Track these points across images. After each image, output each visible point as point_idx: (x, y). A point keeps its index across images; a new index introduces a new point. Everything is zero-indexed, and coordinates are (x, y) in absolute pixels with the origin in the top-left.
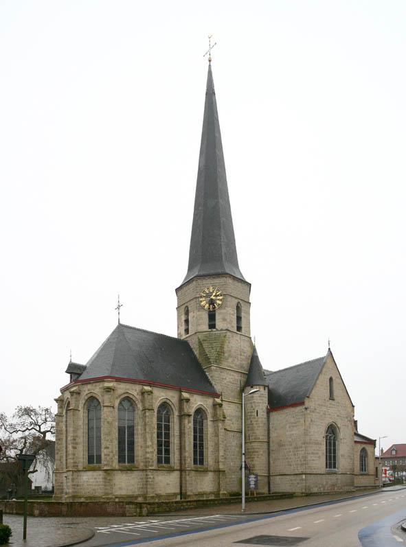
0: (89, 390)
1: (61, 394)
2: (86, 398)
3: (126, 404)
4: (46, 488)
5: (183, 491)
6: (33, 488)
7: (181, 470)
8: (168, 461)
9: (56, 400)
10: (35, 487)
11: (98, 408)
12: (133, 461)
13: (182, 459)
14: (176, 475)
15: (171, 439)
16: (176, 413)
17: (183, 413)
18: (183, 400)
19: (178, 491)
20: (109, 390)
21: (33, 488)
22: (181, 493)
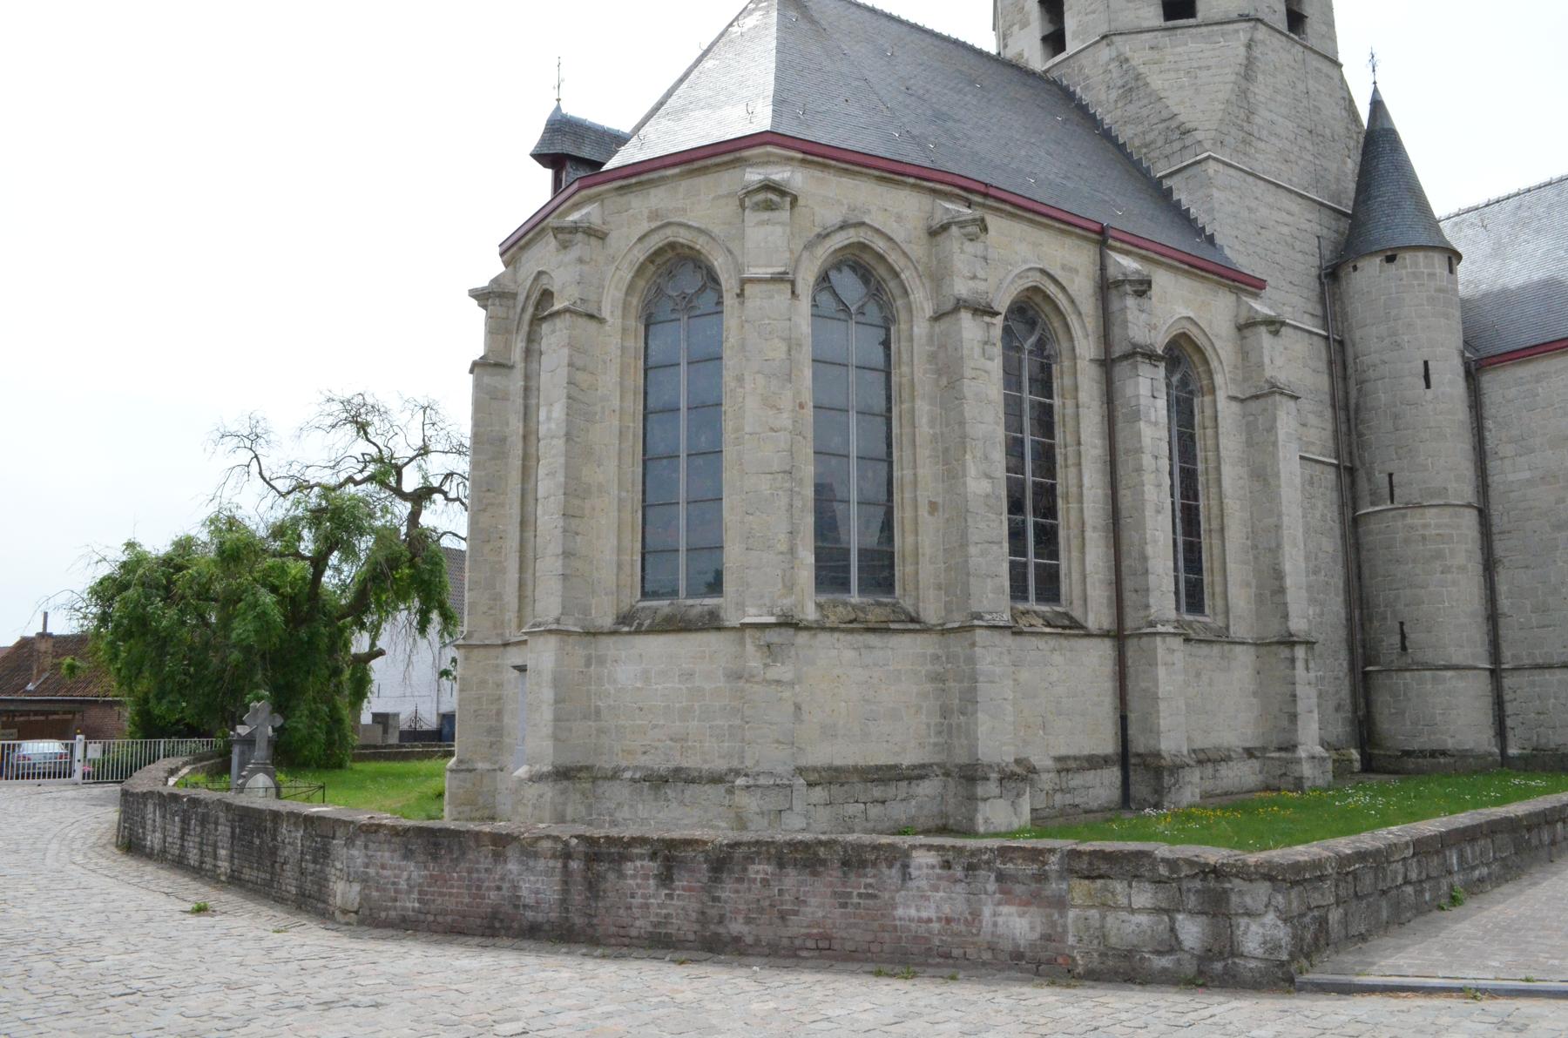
0: (654, 215)
1: (500, 268)
2: (640, 255)
3: (849, 286)
4: (416, 718)
5: (1139, 744)
6: (366, 718)
7: (1119, 636)
8: (1049, 586)
9: (482, 296)
10: (375, 716)
11: (706, 302)
12: (887, 585)
13: (1272, 587)
14: (1096, 657)
15: (1064, 479)
16: (1086, 347)
17: (1117, 352)
18: (1118, 284)
19: (1107, 745)
20: (774, 195)
21: (366, 718)
22: (1125, 757)
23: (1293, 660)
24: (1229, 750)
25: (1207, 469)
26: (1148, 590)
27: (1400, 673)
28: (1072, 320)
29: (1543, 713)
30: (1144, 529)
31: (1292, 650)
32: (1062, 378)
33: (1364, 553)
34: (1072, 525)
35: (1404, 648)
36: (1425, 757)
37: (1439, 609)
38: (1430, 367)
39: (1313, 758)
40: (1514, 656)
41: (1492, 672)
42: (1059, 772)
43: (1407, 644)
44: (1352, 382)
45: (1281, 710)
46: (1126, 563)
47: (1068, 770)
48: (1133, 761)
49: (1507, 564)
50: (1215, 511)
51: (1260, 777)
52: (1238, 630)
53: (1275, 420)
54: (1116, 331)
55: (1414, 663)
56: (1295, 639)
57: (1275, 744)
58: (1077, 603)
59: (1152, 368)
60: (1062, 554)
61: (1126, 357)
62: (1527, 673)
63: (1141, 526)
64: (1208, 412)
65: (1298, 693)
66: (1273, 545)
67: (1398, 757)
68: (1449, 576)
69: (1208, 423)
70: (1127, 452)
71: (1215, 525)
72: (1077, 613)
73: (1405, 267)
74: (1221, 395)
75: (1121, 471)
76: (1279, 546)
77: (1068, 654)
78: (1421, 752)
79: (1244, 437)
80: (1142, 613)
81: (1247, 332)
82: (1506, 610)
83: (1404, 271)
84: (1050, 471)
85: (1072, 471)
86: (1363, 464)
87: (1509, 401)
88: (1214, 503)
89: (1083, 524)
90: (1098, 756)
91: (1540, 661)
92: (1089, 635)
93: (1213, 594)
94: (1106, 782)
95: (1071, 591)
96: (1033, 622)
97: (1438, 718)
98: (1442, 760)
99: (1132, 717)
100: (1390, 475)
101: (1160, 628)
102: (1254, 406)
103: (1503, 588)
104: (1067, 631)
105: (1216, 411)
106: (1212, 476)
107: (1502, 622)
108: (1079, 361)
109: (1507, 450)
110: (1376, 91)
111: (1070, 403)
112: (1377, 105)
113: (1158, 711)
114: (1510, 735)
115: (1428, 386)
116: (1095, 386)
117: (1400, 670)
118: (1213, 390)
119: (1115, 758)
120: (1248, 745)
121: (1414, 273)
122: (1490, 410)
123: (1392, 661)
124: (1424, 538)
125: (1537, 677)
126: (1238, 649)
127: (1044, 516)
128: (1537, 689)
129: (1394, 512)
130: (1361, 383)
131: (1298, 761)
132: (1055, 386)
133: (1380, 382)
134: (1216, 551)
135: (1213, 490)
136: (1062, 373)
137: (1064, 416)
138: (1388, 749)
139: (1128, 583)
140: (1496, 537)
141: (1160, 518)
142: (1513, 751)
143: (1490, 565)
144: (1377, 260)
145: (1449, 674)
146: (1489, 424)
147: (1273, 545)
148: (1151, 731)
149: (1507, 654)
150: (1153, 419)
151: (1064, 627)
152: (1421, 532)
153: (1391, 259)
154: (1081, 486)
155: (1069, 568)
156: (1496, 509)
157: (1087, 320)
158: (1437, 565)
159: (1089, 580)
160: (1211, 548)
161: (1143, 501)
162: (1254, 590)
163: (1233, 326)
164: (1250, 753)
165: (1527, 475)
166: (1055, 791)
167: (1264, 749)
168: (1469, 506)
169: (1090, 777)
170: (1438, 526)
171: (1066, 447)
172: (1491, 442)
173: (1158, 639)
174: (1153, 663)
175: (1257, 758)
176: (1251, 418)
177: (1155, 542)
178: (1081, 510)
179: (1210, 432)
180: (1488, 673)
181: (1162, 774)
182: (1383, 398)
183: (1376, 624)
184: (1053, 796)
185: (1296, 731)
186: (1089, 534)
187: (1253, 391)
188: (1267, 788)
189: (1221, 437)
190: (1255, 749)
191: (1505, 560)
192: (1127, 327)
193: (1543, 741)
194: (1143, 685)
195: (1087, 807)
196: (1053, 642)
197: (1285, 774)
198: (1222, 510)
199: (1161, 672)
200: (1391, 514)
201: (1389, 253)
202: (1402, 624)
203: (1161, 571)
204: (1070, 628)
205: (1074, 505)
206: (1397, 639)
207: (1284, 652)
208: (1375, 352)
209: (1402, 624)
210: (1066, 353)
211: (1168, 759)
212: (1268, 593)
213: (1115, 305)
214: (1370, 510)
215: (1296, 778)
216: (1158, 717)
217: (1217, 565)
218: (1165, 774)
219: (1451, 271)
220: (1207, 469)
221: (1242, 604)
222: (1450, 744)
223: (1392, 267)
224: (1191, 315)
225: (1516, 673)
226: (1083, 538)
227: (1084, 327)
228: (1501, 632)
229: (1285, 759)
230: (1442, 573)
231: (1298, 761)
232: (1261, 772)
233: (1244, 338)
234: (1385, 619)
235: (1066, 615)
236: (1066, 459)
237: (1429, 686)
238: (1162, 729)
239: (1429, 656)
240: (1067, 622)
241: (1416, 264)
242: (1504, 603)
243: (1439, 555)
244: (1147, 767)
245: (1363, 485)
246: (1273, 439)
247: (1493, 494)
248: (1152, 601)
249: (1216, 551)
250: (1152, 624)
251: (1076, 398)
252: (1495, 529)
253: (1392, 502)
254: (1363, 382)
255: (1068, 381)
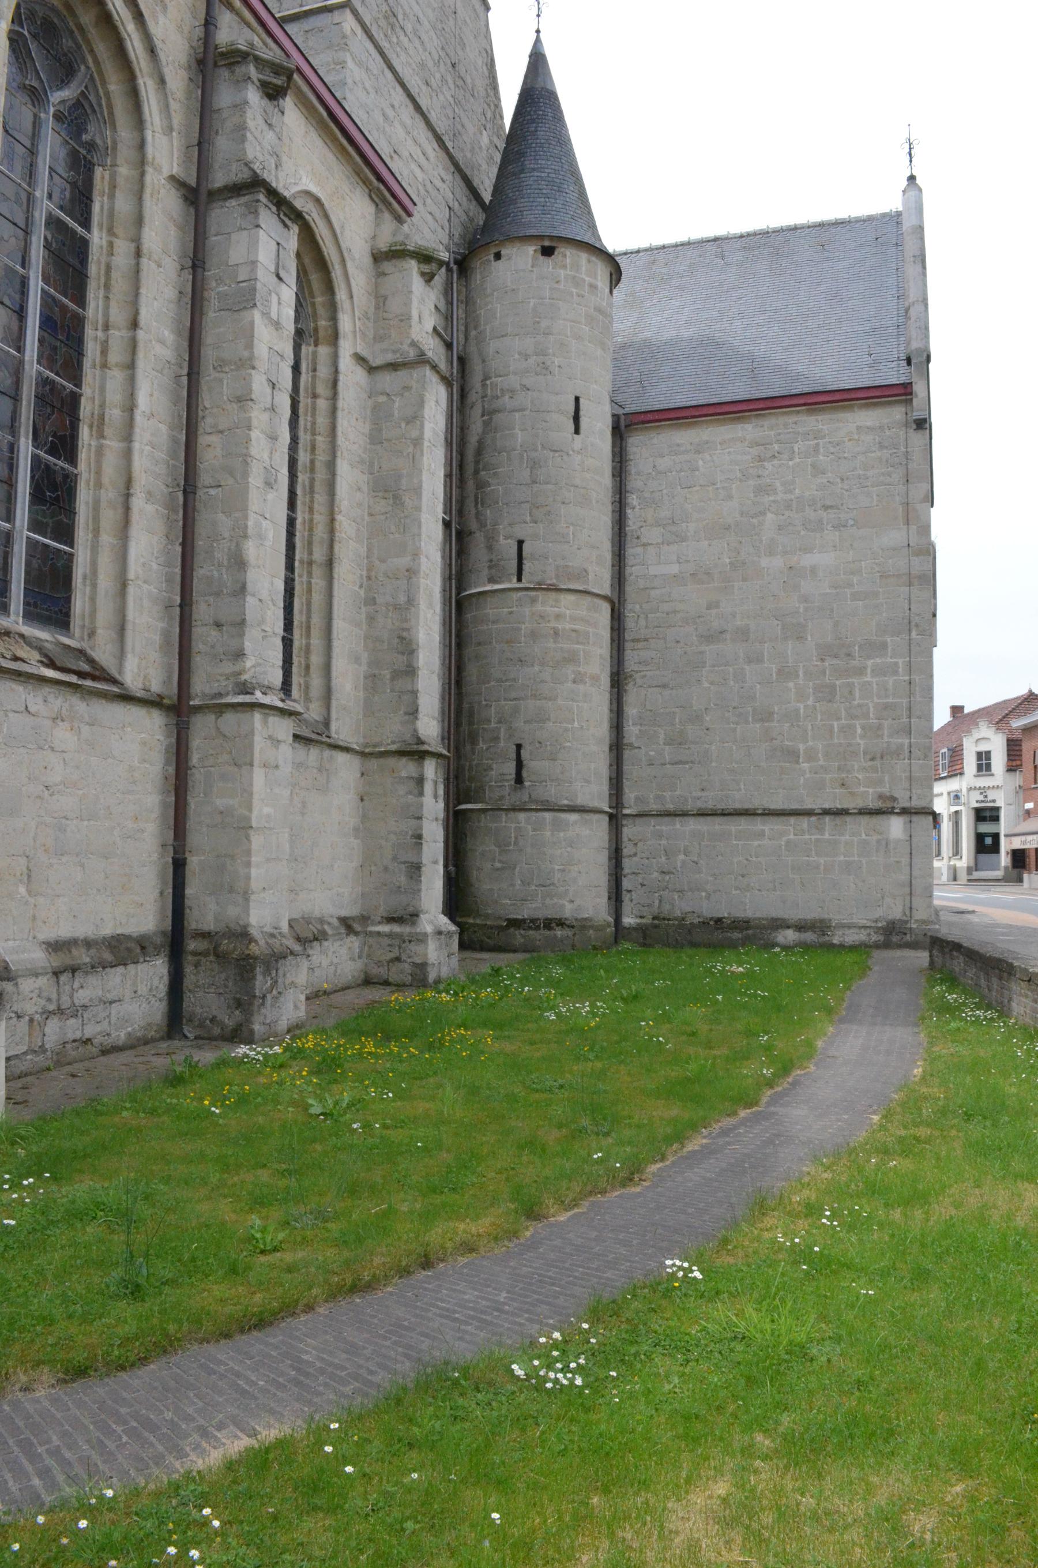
17: (219, 179)
23: (420, 781)
24: (321, 921)
25: (312, 462)
26: (243, 622)
27: (512, 815)
28: (147, 85)
29: (669, 873)
30: (245, 509)
31: (421, 766)
32: (112, 196)
33: (469, 651)
34: (106, 480)
35: (519, 780)
36: (538, 928)
37: (566, 730)
38: (582, 406)
39: (440, 933)
40: (637, 799)
41: (612, 817)
42: (56, 974)
43: (524, 774)
44: (476, 414)
45: (395, 858)
46: (201, 572)
47: (74, 970)
48: (192, 945)
49: (639, 681)
50: (320, 531)
51: (359, 965)
52: (343, 729)
53: (421, 403)
54: (222, 144)
55: (531, 800)
56: (425, 747)
57: (382, 912)
58: (104, 635)
59: (280, 225)
60: (82, 534)
61: (236, 190)
62: (652, 821)
63: (237, 504)
64: (324, 371)
65: (425, 833)
66: (402, 599)
67: (501, 929)
68: (581, 687)
69: (322, 389)
70: (221, 365)
71: (319, 554)
72: (103, 654)
73: (565, 267)
74: (346, 348)
75: (206, 399)
76: (411, 602)
77: (85, 729)
78: (533, 921)
79: (367, 428)
80: (228, 668)
81: (387, 266)
82: (633, 739)
83: (562, 272)
84: (73, 369)
85: (116, 378)
86: (482, 525)
87: (660, 473)
88: (320, 519)
89: (129, 482)
90: (128, 937)
91: (670, 807)
92: (127, 698)
93: (308, 667)
94: (143, 989)
95: (93, 612)
96: (20, 653)
97: (558, 875)
98: (559, 933)
99: (194, 862)
100: (520, 543)
101: (259, 696)
102: (387, 380)
103: (631, 711)
104: (88, 683)
105: (336, 371)
106: (321, 474)
107: (627, 754)
108: (149, 170)
109: (652, 534)
110: (538, 41)
111: (123, 248)
112: (537, 61)
113: (248, 853)
114: (626, 897)
115: (577, 431)
116: (173, 232)
117: (515, 809)
118: (334, 337)
119: (158, 940)
120: (344, 913)
121: (574, 277)
122: (634, 482)
123: (502, 798)
124: (556, 633)
125: (665, 826)
126: (341, 757)
127: (53, 451)
128: (664, 842)
129: (520, 594)
130: (489, 413)
131: (421, 939)
132: (96, 208)
133: (517, 415)
134: (317, 598)
135: (320, 499)
136: (113, 187)
137: (109, 268)
138: (487, 916)
139: (203, 611)
140: (628, 645)
141: (270, 496)
142: (628, 920)
143: (618, 681)
144: (531, 250)
145: (573, 817)
146: (633, 499)
147: (402, 599)
148: (231, 890)
149: (630, 795)
150: (274, 315)
151: (81, 675)
152: (552, 624)
153: (548, 252)
154: (130, 408)
155: (94, 564)
156: (632, 609)
157: (174, 106)
158: (569, 671)
159: (131, 590)
160: (309, 591)
161: (246, 459)
162: (364, 668)
163: (368, 250)
164: (347, 925)
165: (675, 569)
166: (48, 1014)
167: (364, 919)
168: (605, 598)
169: (116, 980)
170: (573, 619)
171: (106, 327)
172: (632, 524)
173: (257, 716)
174: (243, 761)
175: (356, 934)
176: (382, 399)
177: (261, 537)
178: (127, 455)
179: (322, 404)
180: (607, 818)
181: (252, 969)
182: (520, 436)
183: (482, 745)
184: (42, 1026)
185: (419, 890)
186: (138, 502)
187: (390, 358)
188: (368, 981)
189: (340, 414)
190: (353, 919)
191: (637, 676)
192: (243, 139)
193: (667, 907)
194: (220, 803)
195: (108, 1042)
196: (59, 701)
197: (398, 959)
198: (332, 531)
199: (259, 778)
200: (516, 596)
201: (547, 243)
202: (519, 747)
203: (265, 595)
204: (94, 678)
205: (113, 445)
206: (511, 768)
207: (407, 768)
208: (515, 374)
209: (519, 747)
210: (125, 152)
211: (262, 942)
212: (387, 674)
213: (224, 96)
214: (488, 588)
215: (415, 965)
216: (248, 864)
217: (317, 620)
218: (258, 970)
219: (611, 292)
220: (312, 462)
221: (348, 687)
222: (568, 911)
223: (547, 264)
224: (320, 195)
225: (638, 820)
226: (127, 509)
227: (166, 108)
228: (625, 768)
229: (399, 936)
230: (574, 682)
231: (421, 939)
232: (360, 957)
233: (381, 274)
234: (497, 739)
235: (81, 652)
236: (104, 352)
237: (548, 833)
238: (254, 885)
239: (551, 792)
240: (86, 667)
241: (577, 267)
242: (632, 731)
243: (571, 658)
244: (220, 956)
245: (479, 553)
246: (414, 434)
247: (629, 589)
248: (248, 645)
249: (317, 598)
250: (245, 689)
251: (137, 241)
252: (628, 636)
253: (519, 580)
254: (495, 411)
255: (123, 204)
